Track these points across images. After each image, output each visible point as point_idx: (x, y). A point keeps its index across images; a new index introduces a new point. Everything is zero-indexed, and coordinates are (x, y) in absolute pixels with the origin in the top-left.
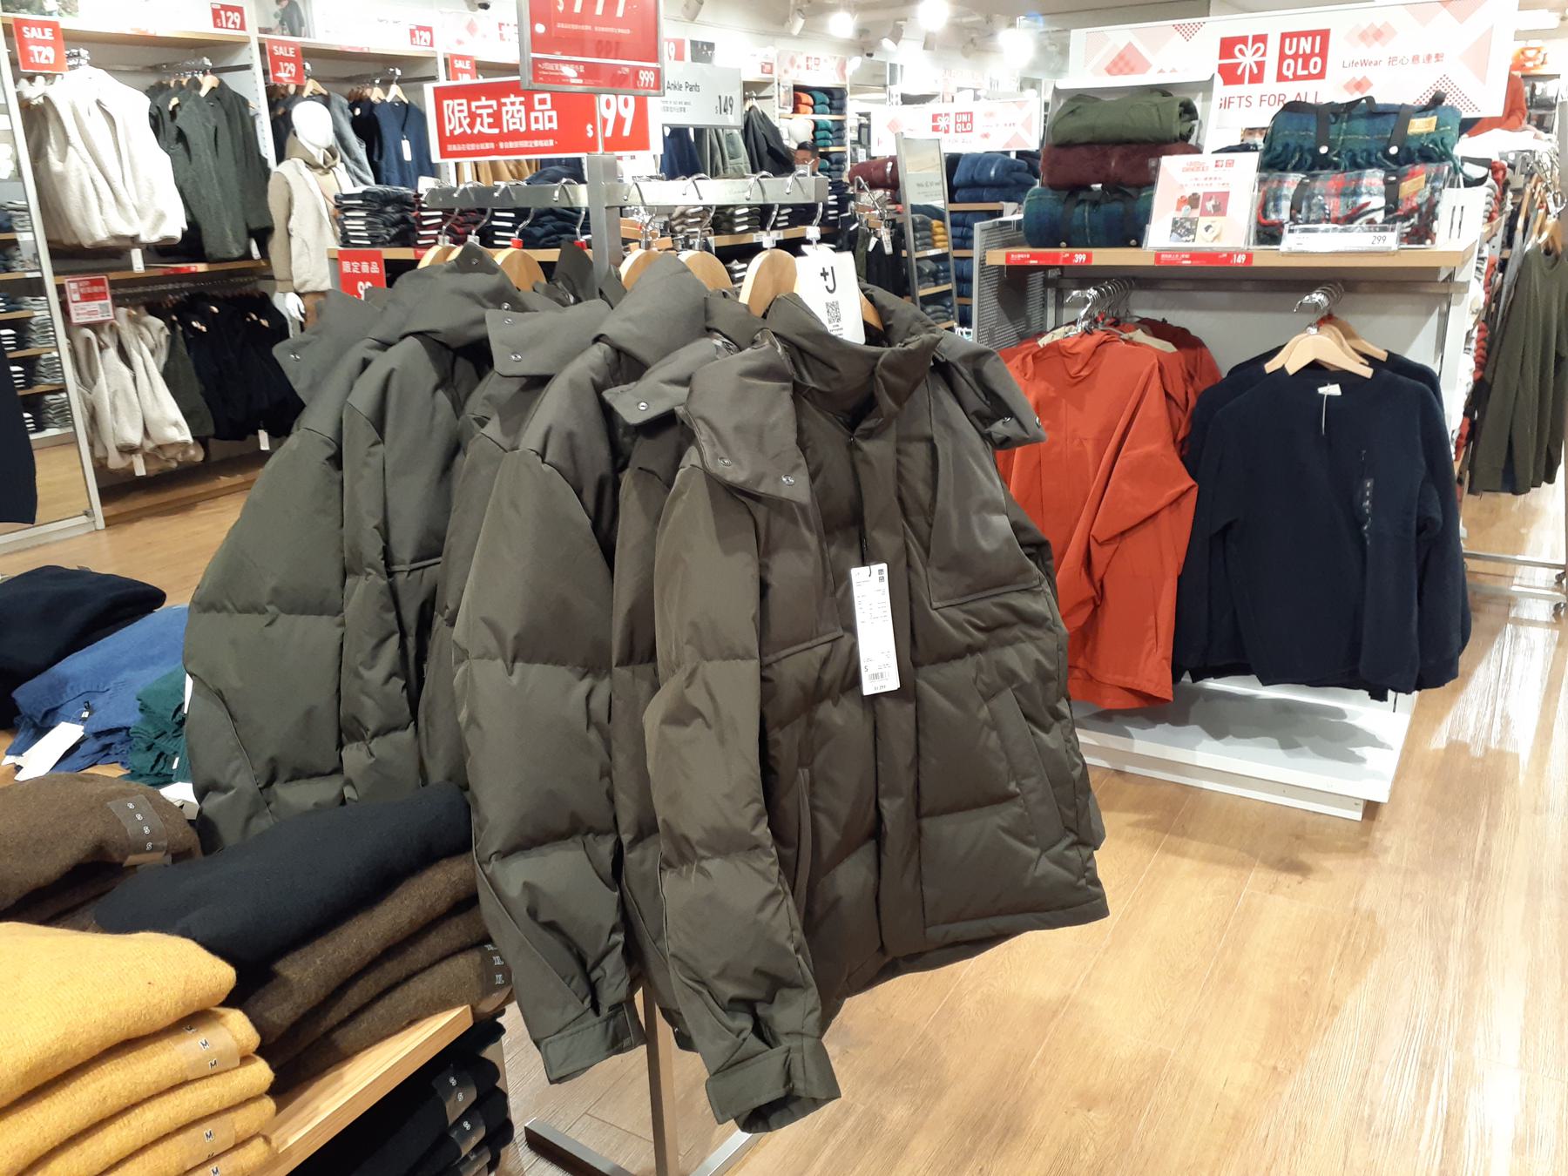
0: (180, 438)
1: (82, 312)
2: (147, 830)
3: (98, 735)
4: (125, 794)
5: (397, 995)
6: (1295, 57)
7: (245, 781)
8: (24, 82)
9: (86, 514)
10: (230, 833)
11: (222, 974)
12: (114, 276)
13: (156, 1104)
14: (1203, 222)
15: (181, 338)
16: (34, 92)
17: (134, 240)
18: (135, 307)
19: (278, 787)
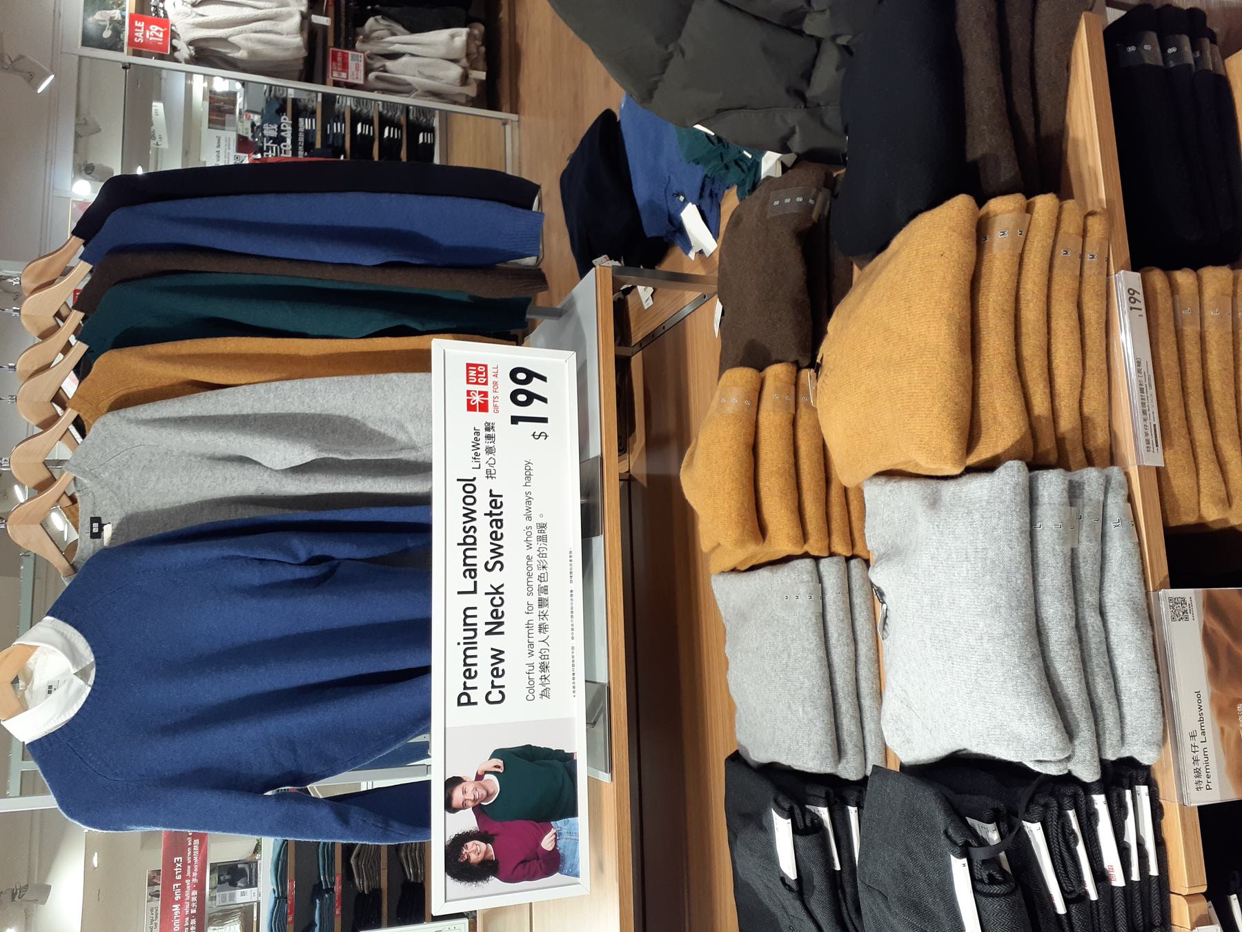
0: (464, 38)
1: (355, 73)
2: (800, 199)
3: (701, 196)
4: (765, 203)
5: (1041, 72)
7: (794, 117)
8: (176, 54)
9: (505, 124)
10: (824, 141)
11: (958, 207)
12: (331, 42)
13: (1024, 278)
15: (386, 9)
16: (185, 52)
17: (305, 17)
18: (356, 35)
19: (809, 94)
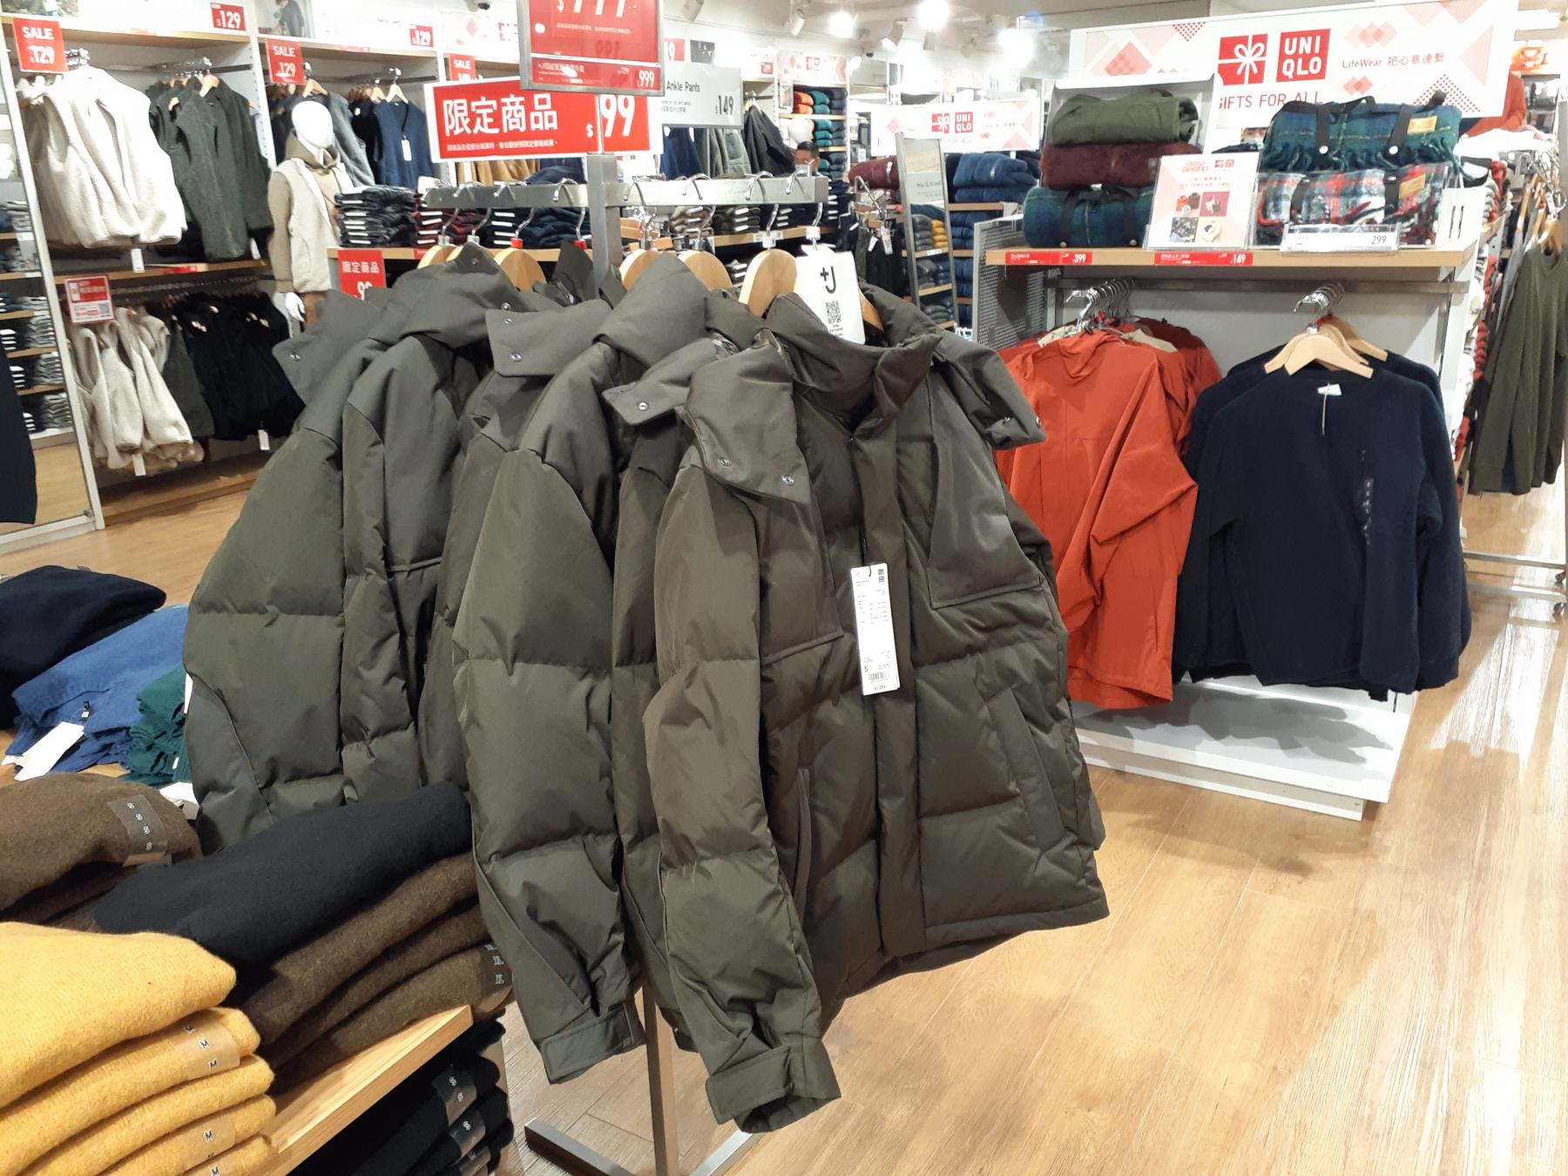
0: (180, 438)
1: (82, 312)
2: (147, 830)
3: (98, 735)
4: (125, 794)
5: (397, 995)
6: (1295, 57)
7: (245, 781)
8: (24, 82)
9: (86, 514)
10: (230, 833)
11: (222, 974)
12: (114, 276)
13: (156, 1104)
14: (1203, 222)
15: (181, 338)
16: (34, 92)
17: (134, 240)
18: (135, 307)
19: (278, 787)
